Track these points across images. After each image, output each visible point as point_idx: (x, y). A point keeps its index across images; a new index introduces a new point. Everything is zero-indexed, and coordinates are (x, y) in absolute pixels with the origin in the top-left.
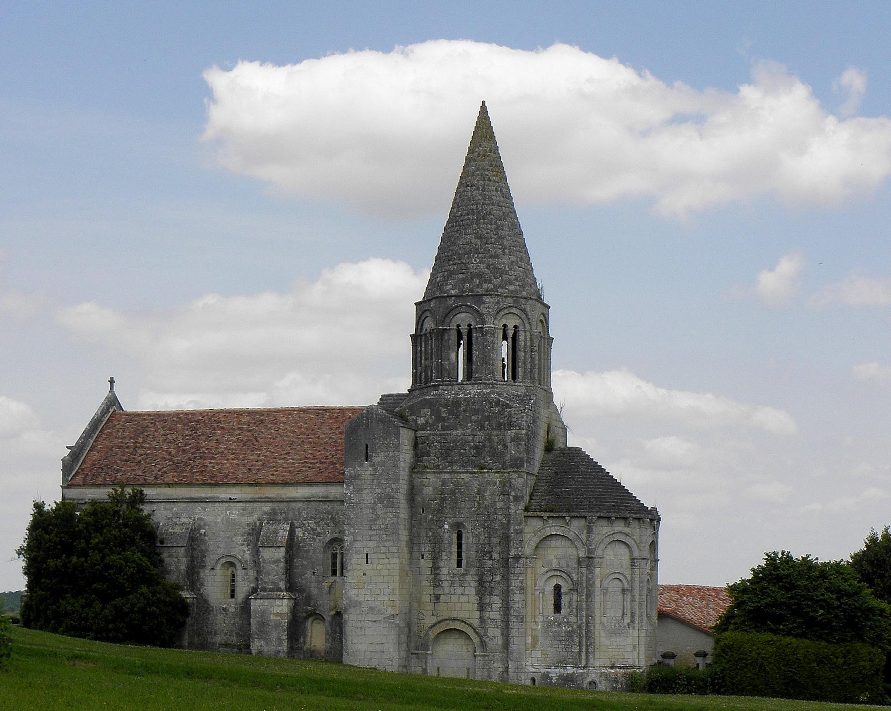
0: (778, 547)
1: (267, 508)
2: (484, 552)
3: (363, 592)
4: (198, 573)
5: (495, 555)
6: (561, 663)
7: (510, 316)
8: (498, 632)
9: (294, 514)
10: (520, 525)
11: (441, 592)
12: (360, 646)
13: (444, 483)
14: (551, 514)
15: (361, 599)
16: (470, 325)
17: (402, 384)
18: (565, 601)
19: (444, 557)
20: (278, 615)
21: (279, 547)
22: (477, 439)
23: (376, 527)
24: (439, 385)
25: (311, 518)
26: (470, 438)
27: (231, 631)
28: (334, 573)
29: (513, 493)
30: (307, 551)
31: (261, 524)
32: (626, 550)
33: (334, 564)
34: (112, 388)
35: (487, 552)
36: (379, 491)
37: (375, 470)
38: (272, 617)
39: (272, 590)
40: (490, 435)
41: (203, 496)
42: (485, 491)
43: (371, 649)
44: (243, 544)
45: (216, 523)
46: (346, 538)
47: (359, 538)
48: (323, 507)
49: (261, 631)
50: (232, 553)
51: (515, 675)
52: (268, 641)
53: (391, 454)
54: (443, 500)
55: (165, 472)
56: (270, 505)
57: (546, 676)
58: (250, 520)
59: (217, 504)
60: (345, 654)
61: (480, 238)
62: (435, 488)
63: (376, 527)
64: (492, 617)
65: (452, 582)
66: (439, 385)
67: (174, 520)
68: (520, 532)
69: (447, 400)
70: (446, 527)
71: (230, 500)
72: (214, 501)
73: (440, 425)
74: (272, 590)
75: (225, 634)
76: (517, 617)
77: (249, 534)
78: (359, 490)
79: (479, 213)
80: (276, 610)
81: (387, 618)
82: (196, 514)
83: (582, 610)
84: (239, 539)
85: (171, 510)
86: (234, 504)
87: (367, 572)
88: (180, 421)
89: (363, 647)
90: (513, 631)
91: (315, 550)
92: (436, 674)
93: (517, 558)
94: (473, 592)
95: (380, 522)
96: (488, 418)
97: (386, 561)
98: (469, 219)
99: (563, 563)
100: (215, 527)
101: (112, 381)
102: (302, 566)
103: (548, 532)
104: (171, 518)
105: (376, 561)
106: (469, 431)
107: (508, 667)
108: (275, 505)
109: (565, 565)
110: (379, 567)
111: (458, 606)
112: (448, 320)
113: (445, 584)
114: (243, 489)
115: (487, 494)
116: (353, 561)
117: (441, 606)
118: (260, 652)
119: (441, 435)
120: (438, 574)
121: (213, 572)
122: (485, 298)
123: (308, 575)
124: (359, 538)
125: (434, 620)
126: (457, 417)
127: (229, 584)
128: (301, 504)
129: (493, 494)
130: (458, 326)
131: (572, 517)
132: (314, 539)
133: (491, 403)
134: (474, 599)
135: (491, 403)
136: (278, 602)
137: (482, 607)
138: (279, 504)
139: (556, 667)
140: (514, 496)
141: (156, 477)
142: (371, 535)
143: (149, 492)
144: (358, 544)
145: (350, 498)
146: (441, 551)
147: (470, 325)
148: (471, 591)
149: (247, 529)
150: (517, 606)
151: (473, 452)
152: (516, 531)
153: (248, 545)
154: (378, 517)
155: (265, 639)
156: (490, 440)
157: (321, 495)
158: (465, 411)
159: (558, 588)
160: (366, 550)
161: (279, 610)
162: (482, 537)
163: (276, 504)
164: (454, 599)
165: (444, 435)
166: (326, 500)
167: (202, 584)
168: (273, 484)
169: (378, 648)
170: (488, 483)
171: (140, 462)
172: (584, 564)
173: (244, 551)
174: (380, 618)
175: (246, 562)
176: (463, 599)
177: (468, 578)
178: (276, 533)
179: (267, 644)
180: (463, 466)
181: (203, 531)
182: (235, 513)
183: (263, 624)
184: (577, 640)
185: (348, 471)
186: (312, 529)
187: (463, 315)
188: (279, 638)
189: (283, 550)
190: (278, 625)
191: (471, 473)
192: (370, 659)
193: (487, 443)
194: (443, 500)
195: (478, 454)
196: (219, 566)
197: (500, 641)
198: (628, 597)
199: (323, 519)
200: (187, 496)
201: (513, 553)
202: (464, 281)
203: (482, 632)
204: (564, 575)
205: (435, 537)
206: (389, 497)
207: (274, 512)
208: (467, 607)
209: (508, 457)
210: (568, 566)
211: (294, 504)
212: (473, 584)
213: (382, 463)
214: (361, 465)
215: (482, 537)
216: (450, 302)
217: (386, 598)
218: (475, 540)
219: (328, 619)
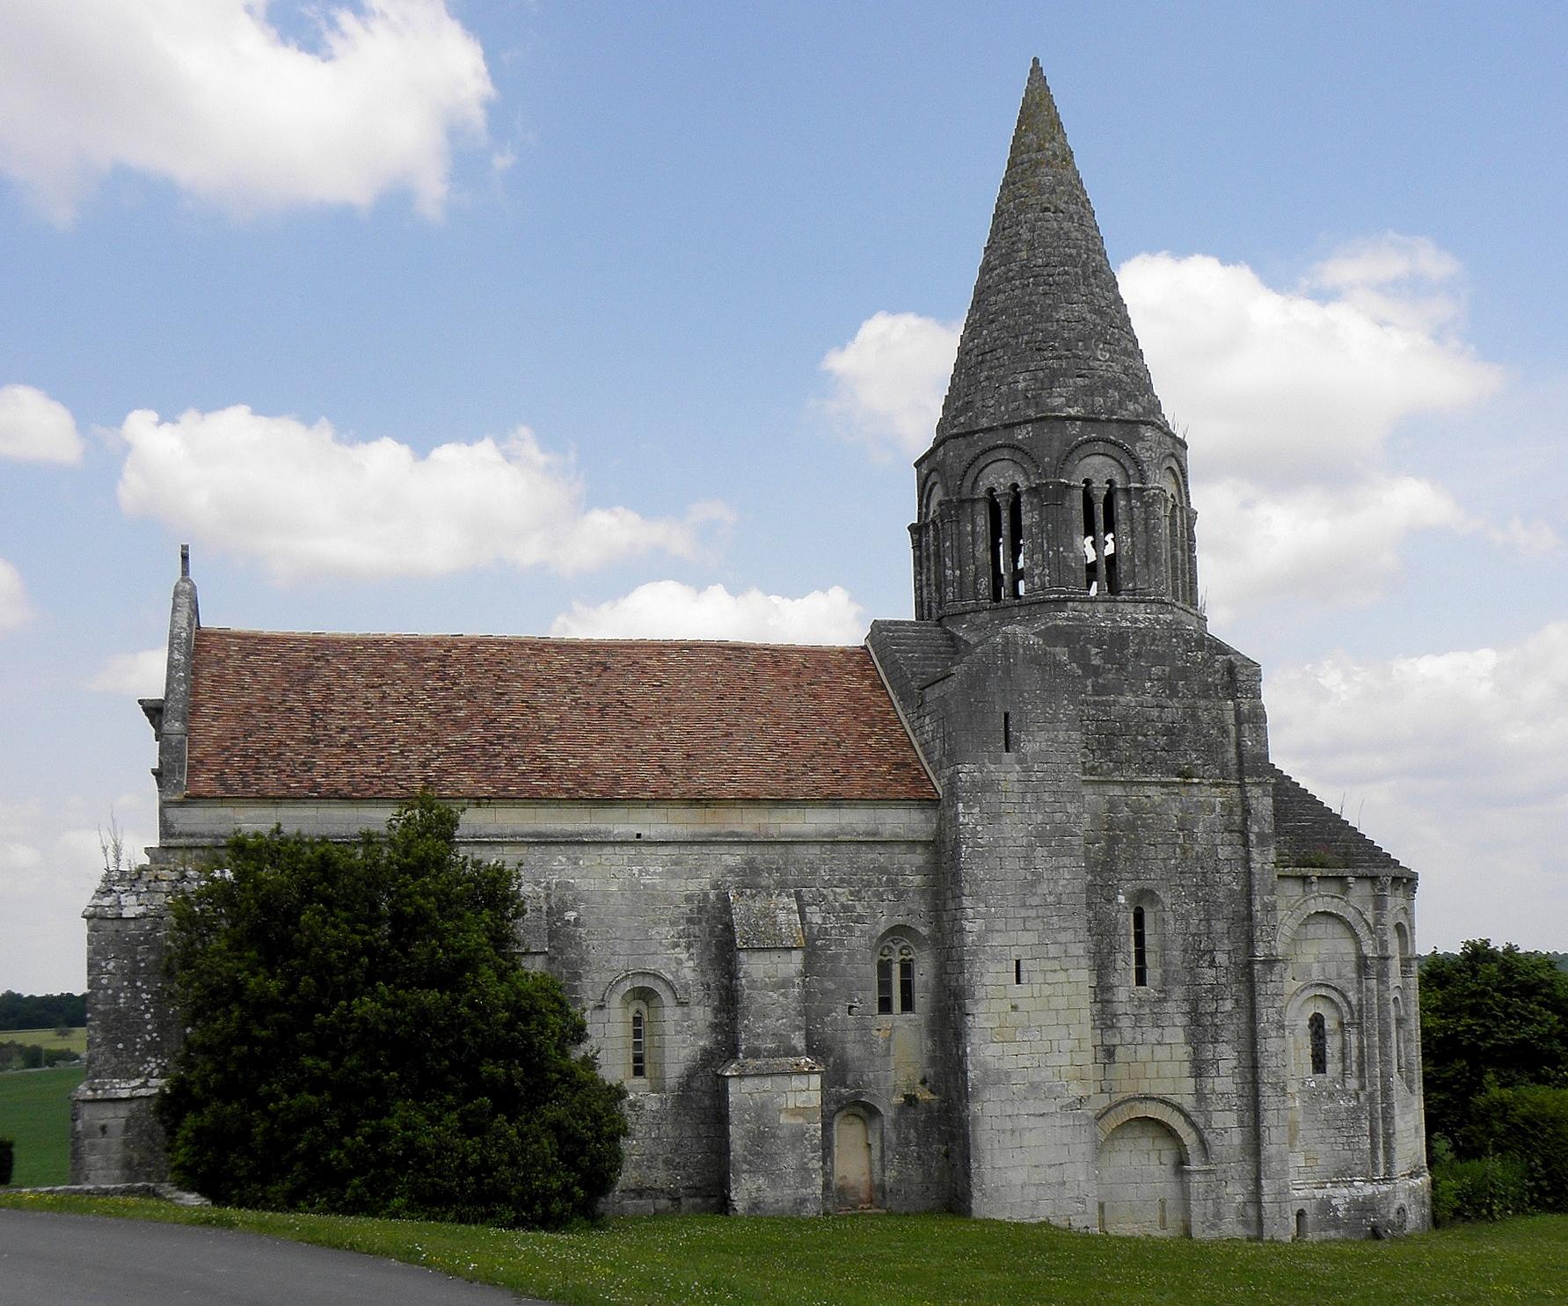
0: (1476, 937)
1: (734, 858)
2: (1200, 953)
3: (1012, 1049)
5: (1221, 958)
6: (1343, 1175)
9: (801, 871)
10: (1272, 893)
11: (1116, 1041)
13: (1113, 806)
14: (1325, 872)
17: (904, 609)
18: (1333, 1045)
19: (1120, 964)
20: (797, 1111)
21: (789, 949)
22: (1168, 715)
23: (1035, 901)
24: (1066, 601)
25: (842, 881)
26: (1155, 713)
27: (653, 1157)
30: (836, 958)
31: (724, 899)
33: (885, 986)
34: (185, 572)
35: (1205, 952)
37: (1027, 770)
38: (783, 1119)
39: (773, 1054)
40: (1194, 708)
41: (569, 828)
42: (1195, 823)
43: (1036, 1179)
44: (676, 945)
46: (968, 926)
47: (999, 925)
48: (868, 856)
49: (758, 1154)
50: (651, 967)
51: (1275, 1207)
52: (776, 1178)
53: (1062, 736)
56: (742, 850)
57: (1326, 1206)
58: (693, 887)
59: (608, 850)
60: (976, 1194)
61: (1099, 312)
62: (1095, 816)
63: (1035, 901)
64: (1218, 1089)
65: (1138, 1018)
66: (1066, 601)
68: (1271, 909)
70: (1121, 899)
71: (639, 841)
72: (602, 842)
73: (1089, 682)
74: (773, 1054)
75: (638, 1166)
76: (1274, 1086)
77: (690, 920)
78: (995, 817)
79: (1085, 264)
80: (792, 1101)
81: (1069, 1106)
82: (553, 872)
83: (1372, 1064)
84: (666, 932)
86: (652, 849)
87: (1018, 1002)
89: (1018, 1177)
90: (1269, 1114)
91: (852, 955)
92: (1232, 1228)
93: (1270, 962)
94: (1180, 1036)
95: (1043, 888)
96: (1184, 674)
97: (1061, 976)
98: (1066, 273)
99: (1332, 969)
100: (611, 898)
102: (824, 992)
105: (1039, 978)
106: (1148, 697)
108: (754, 852)
109: (1334, 975)
110: (1047, 990)
111: (1151, 1070)
112: (1068, 467)
113: (1125, 1023)
115: (1199, 830)
116: (987, 979)
117: (1119, 1071)
118: (755, 1205)
120: (1109, 1001)
121: (599, 1015)
122: (1143, 429)
123: (839, 1013)
124: (999, 925)
126: (1122, 667)
128: (816, 850)
129: (1211, 831)
132: (850, 930)
133: (1187, 642)
134: (1183, 1052)
135: (1187, 642)
136: (796, 1082)
137: (1199, 1069)
138: (765, 849)
139: (1335, 1184)
140: (1257, 835)
144: (996, 940)
145: (974, 833)
146: (1113, 950)
148: (1176, 1035)
149: (686, 908)
151: (1163, 740)
152: (1264, 905)
153: (689, 946)
154: (1038, 879)
155: (767, 1173)
156: (1194, 717)
157: (862, 828)
158: (1137, 655)
159: (1317, 1022)
160: (1015, 953)
161: (800, 1100)
162: (1194, 921)
164: (1143, 1053)
165: (1102, 703)
166: (874, 842)
168: (752, 801)
169: (1053, 1175)
170: (1200, 806)
172: (1373, 972)
173: (679, 962)
175: (686, 988)
176: (1162, 1053)
177: (1170, 1007)
178: (768, 915)
179: (773, 1184)
180: (1145, 771)
181: (571, 915)
182: (654, 870)
183: (761, 1138)
184: (1366, 1125)
185: (967, 772)
186: (845, 908)
187: (1097, 460)
188: (803, 1168)
189: (797, 956)
190: (799, 1136)
191: (1164, 785)
192: (1036, 1203)
193: (1189, 724)
194: (1113, 841)
195: (1171, 747)
196: (615, 1001)
197: (1236, 1138)
199: (869, 884)
200: (527, 829)
201: (1260, 952)
202: (1090, 391)
203: (1200, 1121)
205: (1100, 922)
206: (1063, 832)
207: (751, 869)
208: (1169, 1069)
210: (1340, 976)
211: (800, 851)
212: (1180, 1020)
213: (1042, 757)
214: (997, 760)
215: (1194, 921)
216: (1074, 429)
217: (1065, 1060)
218: (1181, 926)
219: (888, 1113)
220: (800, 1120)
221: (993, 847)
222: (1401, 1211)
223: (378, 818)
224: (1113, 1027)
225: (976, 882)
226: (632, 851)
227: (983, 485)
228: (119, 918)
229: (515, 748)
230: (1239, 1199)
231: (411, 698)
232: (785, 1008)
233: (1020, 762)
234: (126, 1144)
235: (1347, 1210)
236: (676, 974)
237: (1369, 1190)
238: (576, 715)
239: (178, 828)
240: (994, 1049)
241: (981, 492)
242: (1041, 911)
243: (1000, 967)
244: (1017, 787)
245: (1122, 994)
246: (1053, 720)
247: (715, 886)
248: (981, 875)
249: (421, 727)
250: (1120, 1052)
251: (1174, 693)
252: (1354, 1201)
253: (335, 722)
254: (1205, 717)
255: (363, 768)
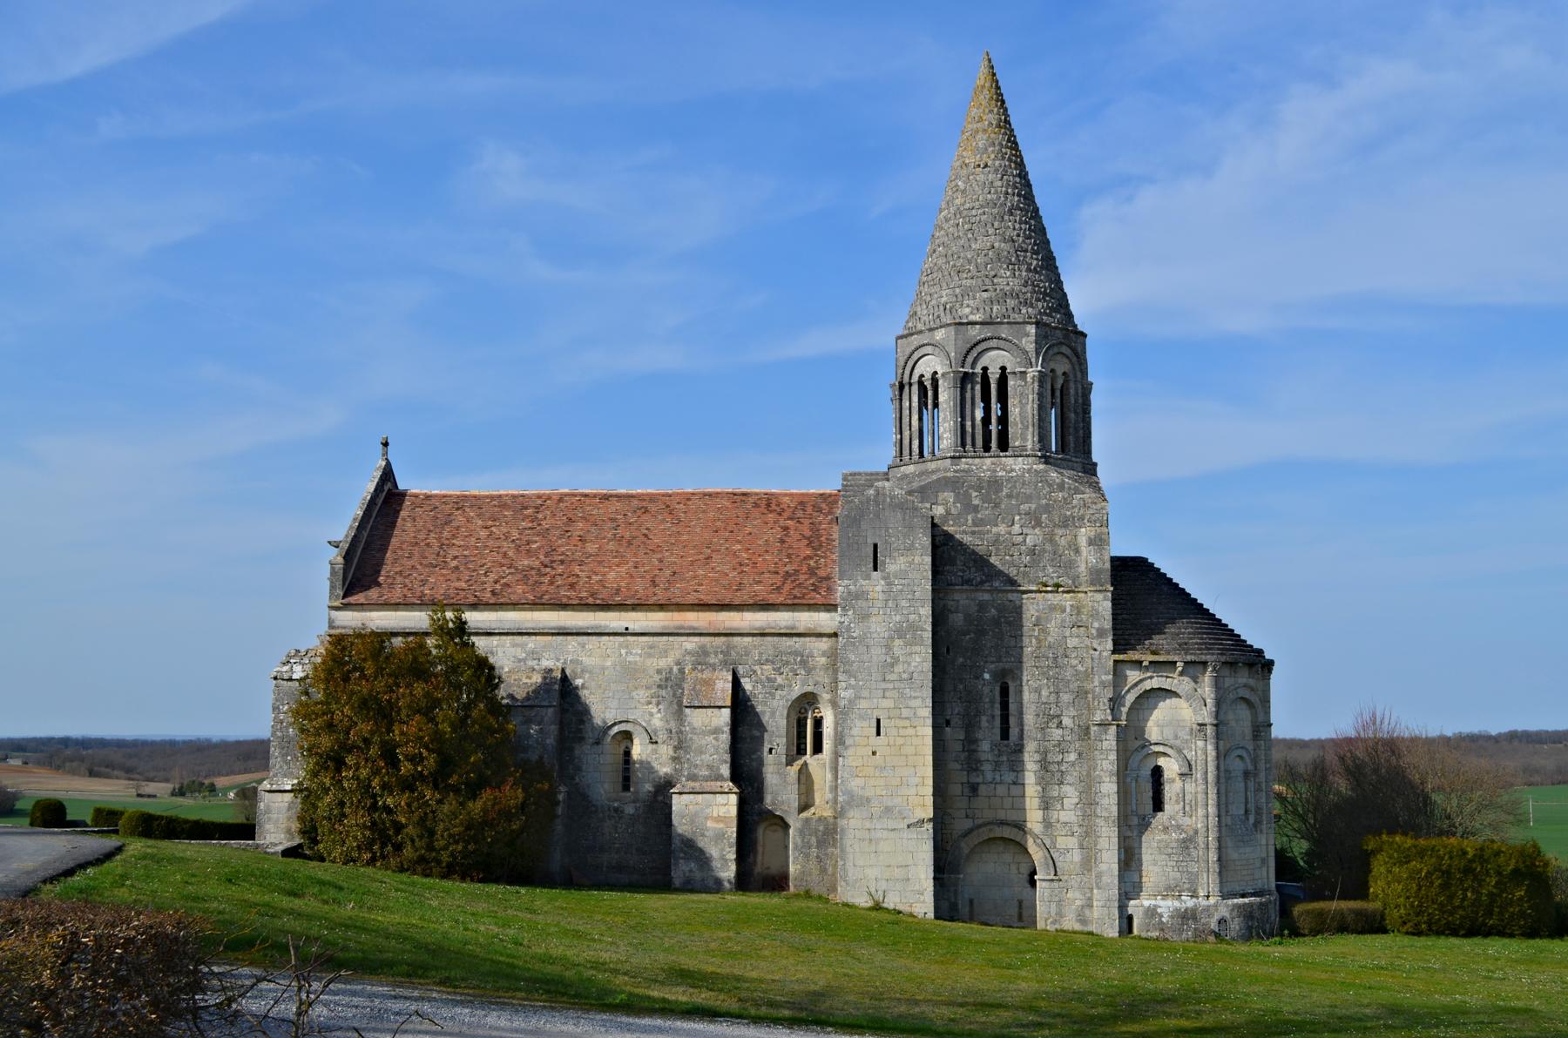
1: (691, 644)
3: (872, 782)
4: (572, 750)
5: (1066, 721)
7: (1059, 357)
8: (1072, 842)
11: (980, 780)
12: (868, 871)
15: (869, 793)
16: (1003, 369)
18: (1171, 791)
20: (719, 819)
26: (1020, 538)
28: (801, 751)
29: (1096, 625)
31: (682, 671)
32: (1248, 713)
35: (1054, 717)
36: (898, 618)
37: (889, 584)
38: (709, 824)
39: (707, 779)
42: (1048, 620)
45: (603, 669)
47: (865, 693)
50: (631, 717)
54: (981, 632)
55: (507, 585)
56: (696, 639)
58: (663, 663)
64: (1062, 819)
67: (530, 663)
69: (979, 478)
70: (987, 676)
71: (626, 633)
74: (707, 779)
77: (659, 686)
78: (865, 617)
84: (642, 694)
85: (523, 646)
88: (504, 506)
95: (899, 668)
96: (1047, 509)
97: (911, 731)
101: (386, 444)
103: (1148, 685)
104: (524, 660)
105: (894, 732)
107: (1090, 899)
110: (900, 741)
112: (970, 359)
113: (987, 767)
114: (650, 615)
116: (855, 731)
119: (973, 533)
124: (865, 693)
125: (968, 824)
126: (997, 505)
127: (621, 767)
130: (985, 369)
131: (1186, 663)
132: (773, 696)
136: (720, 798)
139: (1165, 897)
141: (493, 593)
142: (884, 690)
143: (474, 618)
144: (863, 704)
146: (978, 713)
147: (1003, 369)
149: (657, 678)
150: (1105, 801)
153: (658, 704)
154: (896, 661)
156: (1051, 541)
157: (783, 624)
158: (1009, 496)
160: (876, 714)
161: (722, 811)
162: (1044, 693)
163: (708, 639)
164: (1001, 790)
165: (980, 532)
167: (579, 769)
170: (1053, 608)
171: (457, 568)
173: (651, 714)
174: (903, 825)
175: (655, 732)
178: (709, 683)
185: (841, 588)
186: (769, 680)
189: (726, 713)
190: (720, 836)
193: (1048, 547)
197: (1077, 856)
198: (1251, 785)
199: (787, 663)
203: (1048, 843)
204: (1169, 751)
206: (914, 628)
207: (704, 652)
209: (1082, 568)
210: (1176, 737)
213: (902, 574)
214: (868, 577)
220: (721, 826)
221: (862, 639)
222: (1222, 921)
223: (418, 619)
224: (977, 770)
225: (849, 663)
226: (621, 639)
227: (984, 361)
228: (290, 679)
229: (560, 569)
230: (1078, 903)
231: (507, 536)
232: (717, 749)
233: (884, 578)
234: (289, 819)
235: (1172, 917)
236: (649, 722)
237: (1190, 903)
238: (611, 546)
239: (337, 623)
240: (859, 782)
241: (915, 378)
242: (897, 685)
243: (865, 724)
244: (881, 596)
245: (985, 746)
246: (910, 549)
247: (678, 663)
248: (853, 657)
249: (505, 554)
250: (982, 788)
251: (1038, 524)
252: (1177, 910)
253: (453, 552)
254: (1063, 542)
255: (457, 584)
